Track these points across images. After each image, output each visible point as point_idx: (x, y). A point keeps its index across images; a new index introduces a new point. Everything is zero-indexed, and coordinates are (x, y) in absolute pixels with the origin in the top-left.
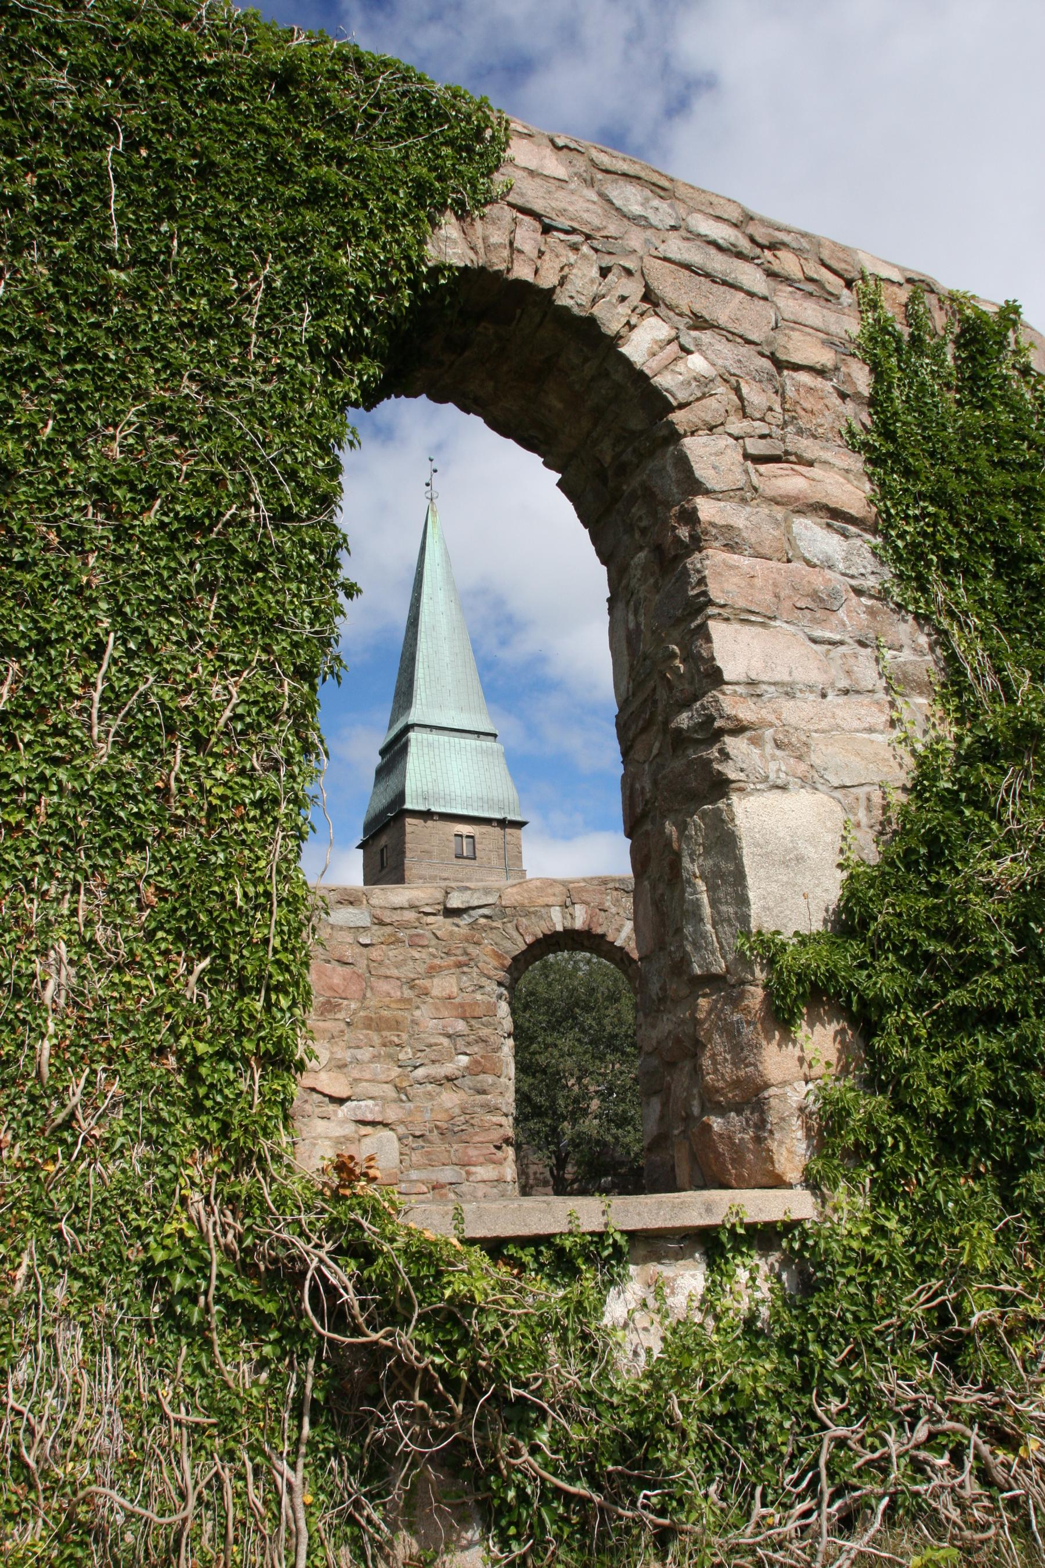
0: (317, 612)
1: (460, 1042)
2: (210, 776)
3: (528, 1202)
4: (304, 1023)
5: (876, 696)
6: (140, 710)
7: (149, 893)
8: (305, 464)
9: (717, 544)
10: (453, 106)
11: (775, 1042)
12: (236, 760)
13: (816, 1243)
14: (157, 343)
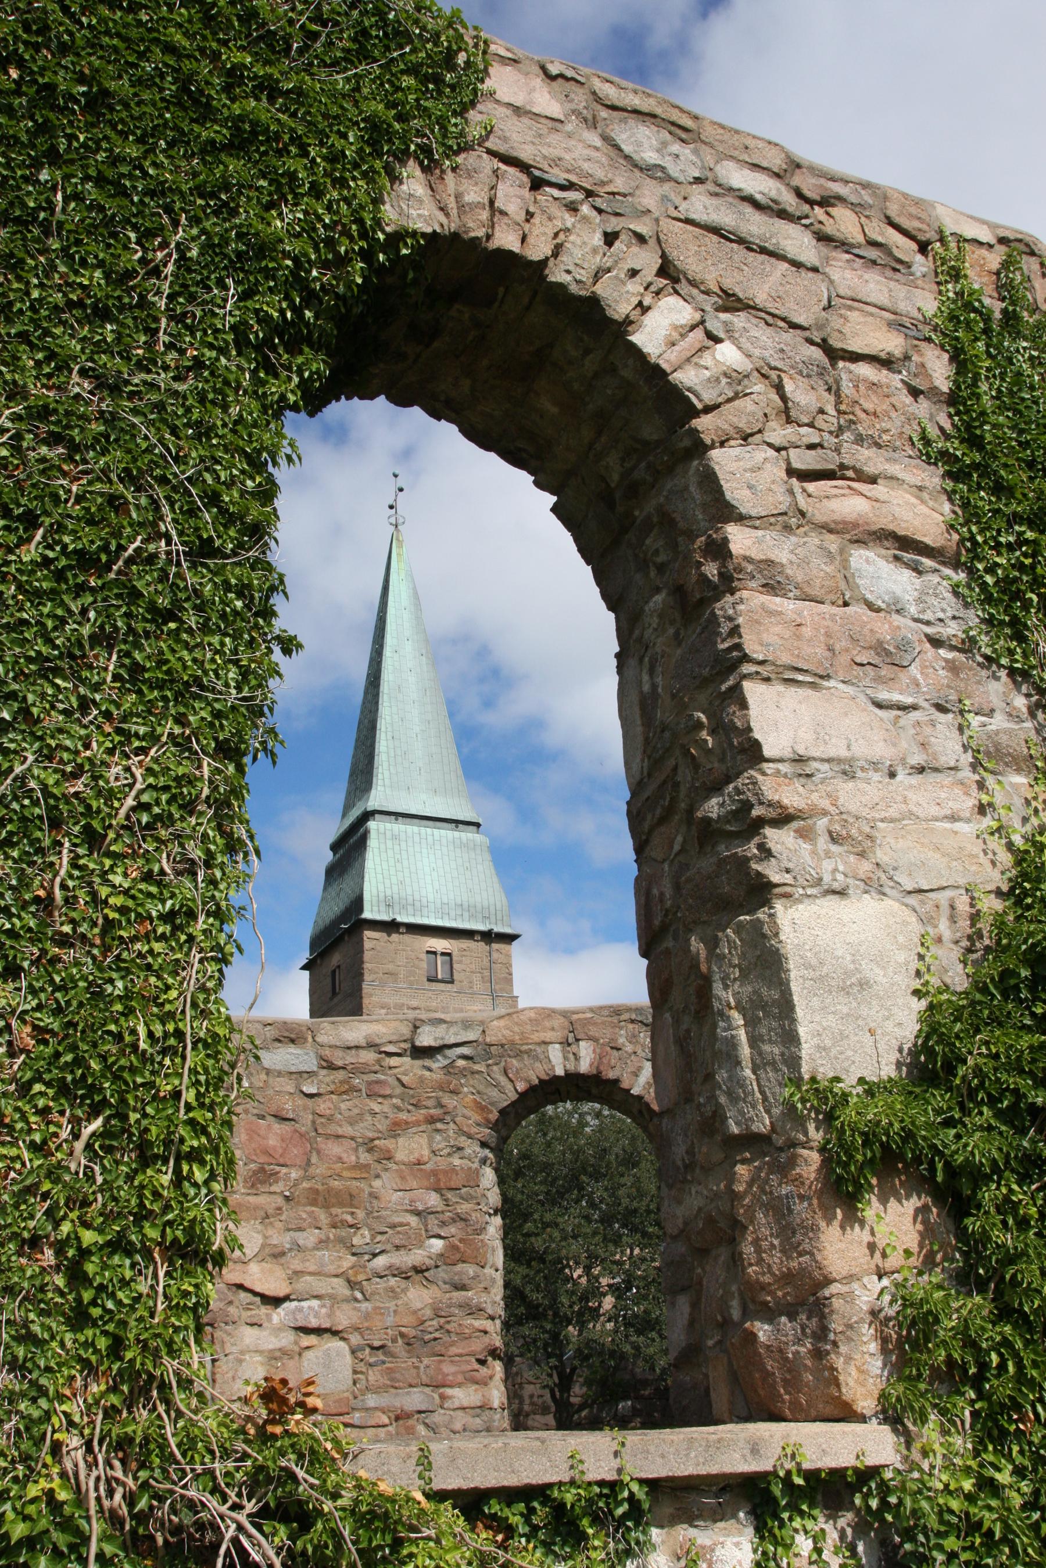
0: (245, 673)
1: (433, 1221)
2: (106, 882)
3: (519, 1440)
4: (224, 1201)
5: (960, 775)
6: (16, 798)
7: (24, 1034)
8: (230, 484)
9: (753, 584)
10: (416, 22)
11: (836, 1223)
12: (141, 862)
13: (901, 1502)
14: (38, 327)
